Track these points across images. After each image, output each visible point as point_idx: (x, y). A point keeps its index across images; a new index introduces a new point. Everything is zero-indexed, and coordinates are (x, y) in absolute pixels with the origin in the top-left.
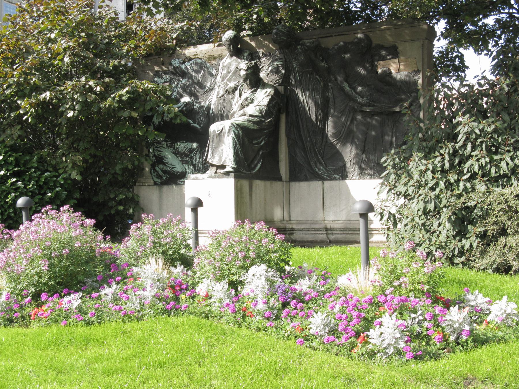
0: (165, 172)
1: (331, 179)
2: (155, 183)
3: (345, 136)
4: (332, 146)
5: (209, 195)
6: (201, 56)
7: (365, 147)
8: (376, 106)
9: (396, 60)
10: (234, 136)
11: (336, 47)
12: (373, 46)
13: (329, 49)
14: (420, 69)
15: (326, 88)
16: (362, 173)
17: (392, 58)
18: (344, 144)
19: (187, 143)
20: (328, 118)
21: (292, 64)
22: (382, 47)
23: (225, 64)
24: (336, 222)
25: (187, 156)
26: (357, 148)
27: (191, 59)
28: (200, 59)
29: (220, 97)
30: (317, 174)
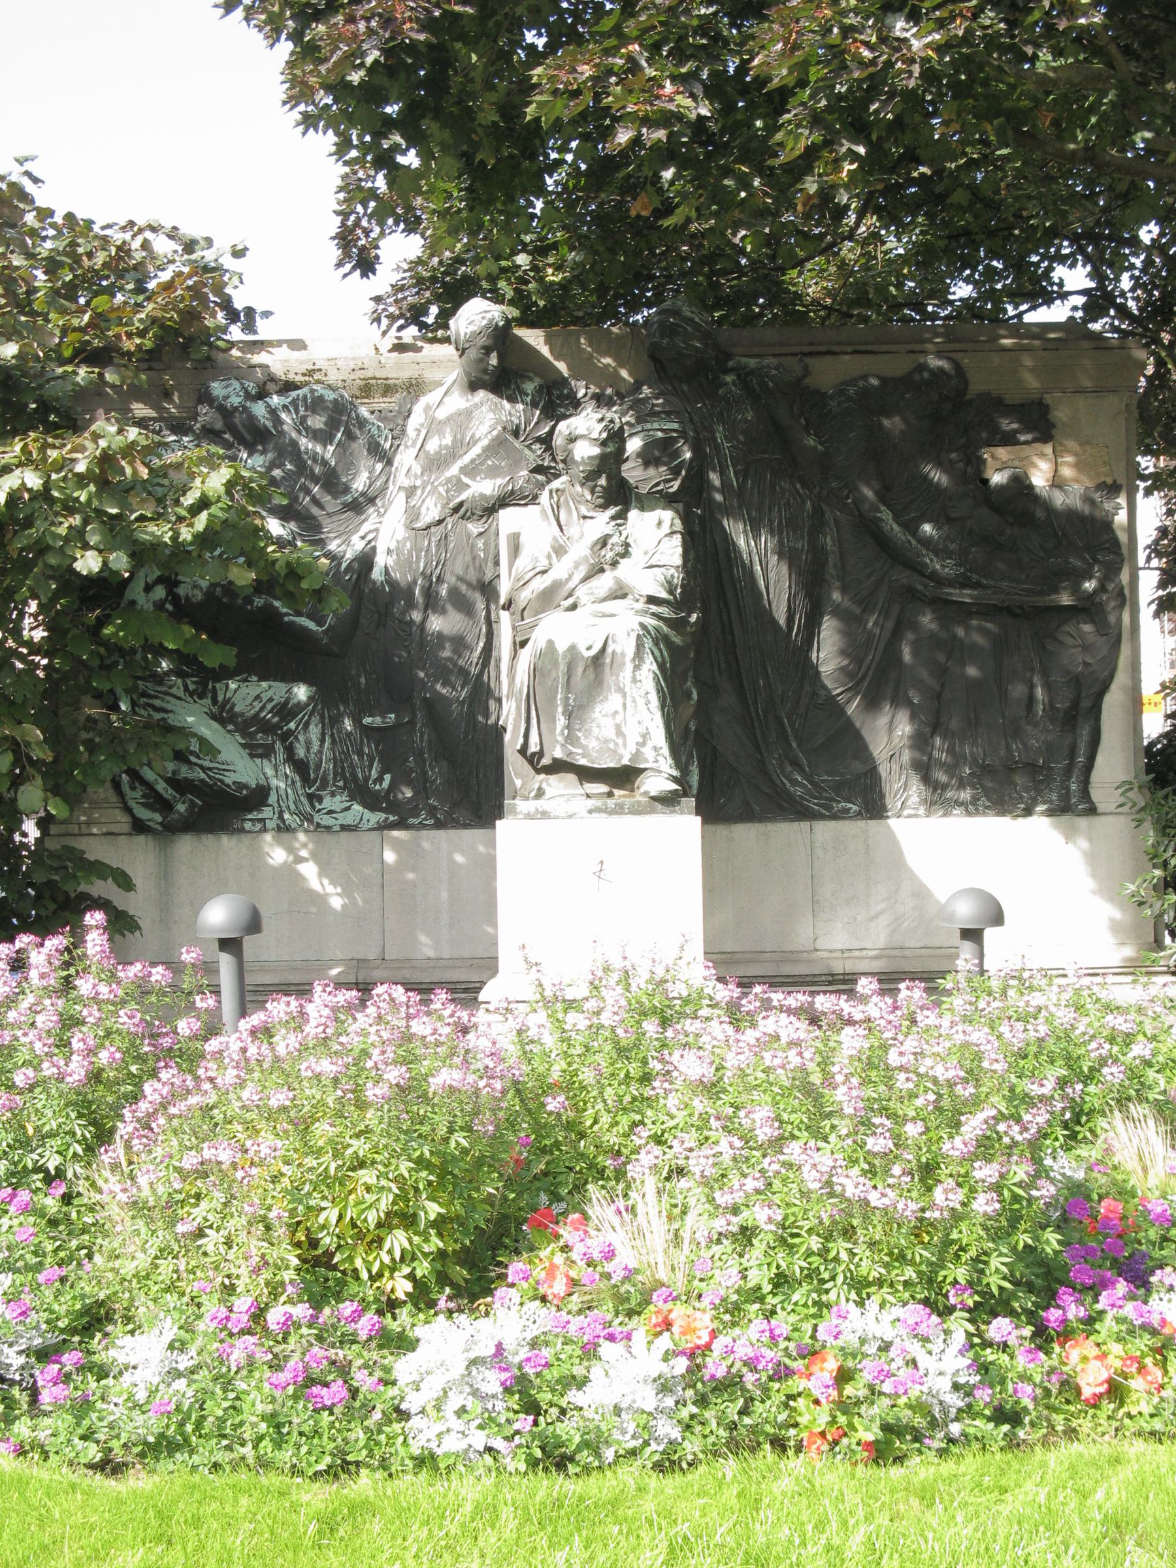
0: (181, 786)
1: (835, 817)
2: (139, 827)
3: (878, 680)
4: (835, 709)
5: (599, 873)
6: (333, 378)
7: (938, 711)
8: (986, 587)
9: (1048, 449)
10: (655, 667)
11: (852, 391)
12: (968, 397)
13: (823, 395)
14: (1122, 481)
15: (818, 522)
16: (938, 799)
17: (1035, 440)
18: (872, 704)
19: (264, 684)
20: (822, 616)
21: (713, 432)
22: (999, 405)
23: (441, 414)
24: (857, 953)
25: (267, 728)
26: (913, 717)
27: (288, 387)
28: (330, 387)
29: (428, 527)
30: (790, 798)
